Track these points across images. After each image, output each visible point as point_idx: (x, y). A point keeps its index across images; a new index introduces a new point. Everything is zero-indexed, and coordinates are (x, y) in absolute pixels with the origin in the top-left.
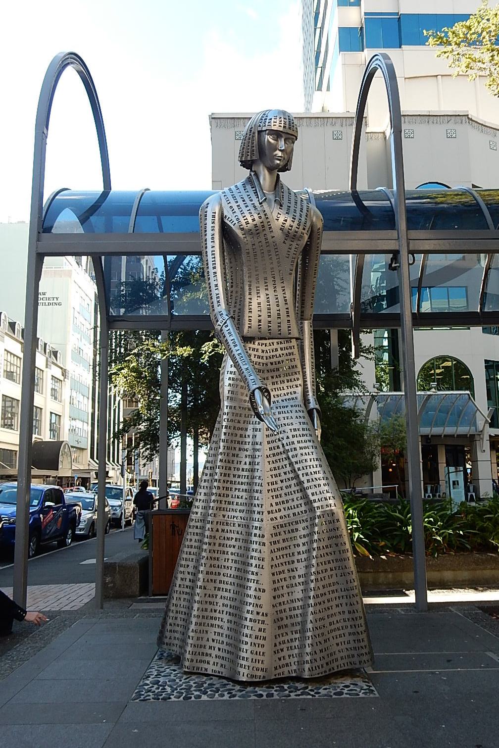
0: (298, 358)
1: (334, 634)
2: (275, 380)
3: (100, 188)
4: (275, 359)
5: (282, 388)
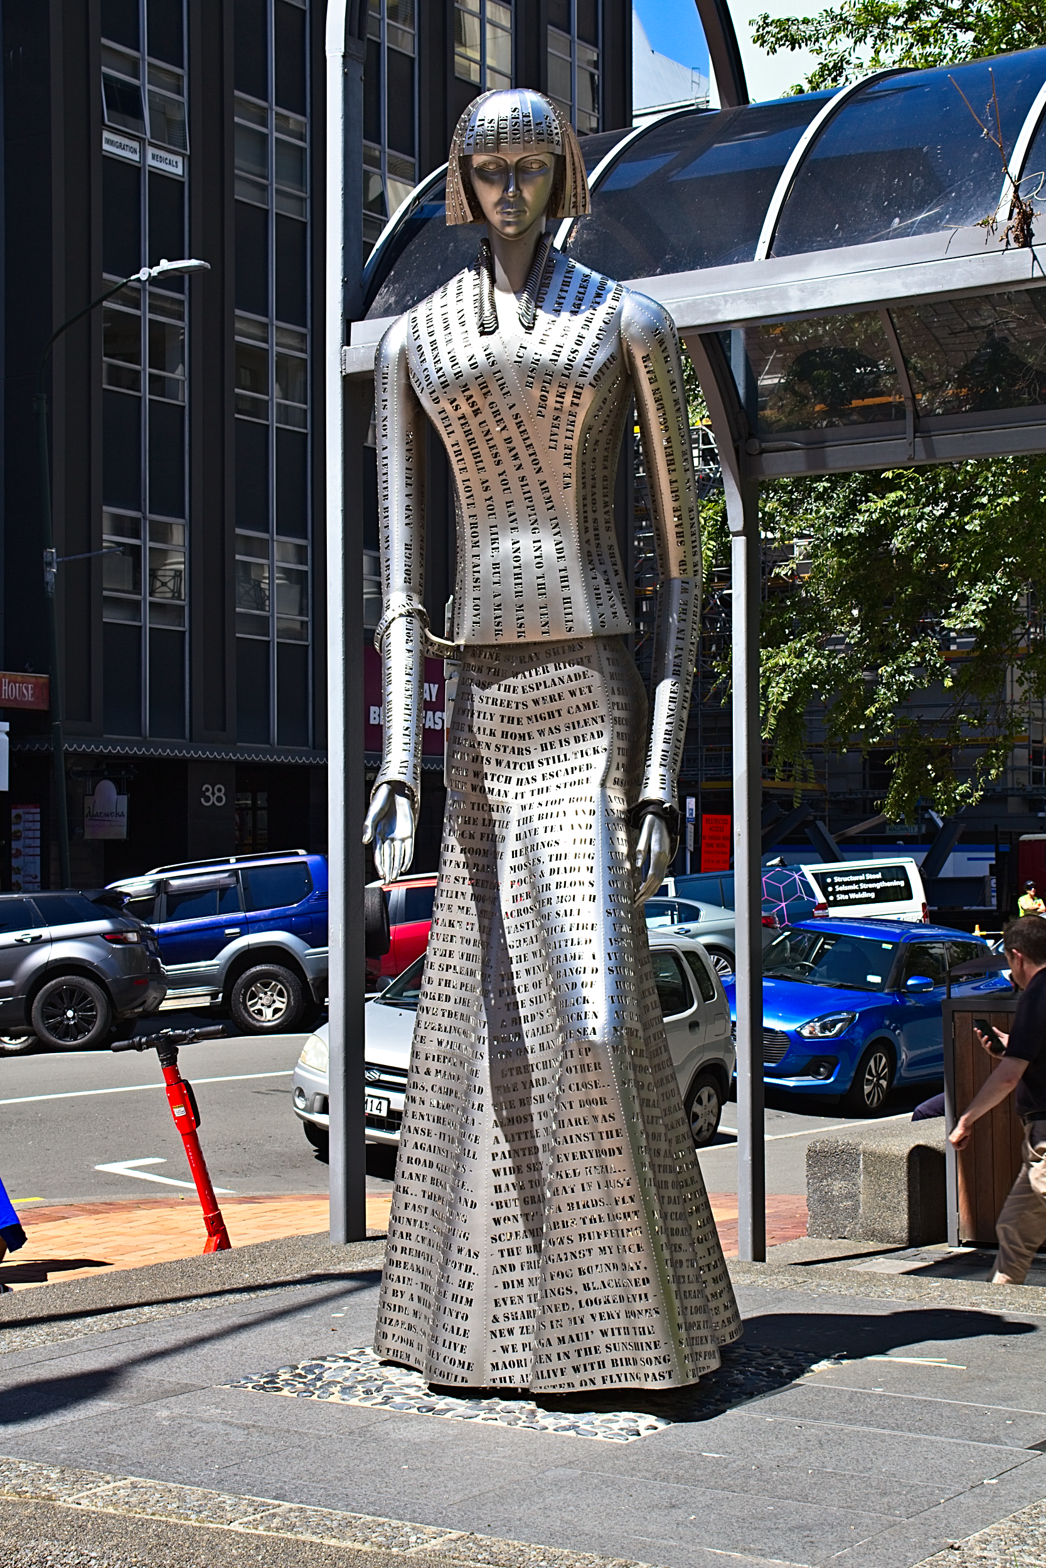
0: (601, 963)
1: (595, 1309)
2: (547, 739)
3: (354, 326)
4: (543, 692)
5: (562, 758)
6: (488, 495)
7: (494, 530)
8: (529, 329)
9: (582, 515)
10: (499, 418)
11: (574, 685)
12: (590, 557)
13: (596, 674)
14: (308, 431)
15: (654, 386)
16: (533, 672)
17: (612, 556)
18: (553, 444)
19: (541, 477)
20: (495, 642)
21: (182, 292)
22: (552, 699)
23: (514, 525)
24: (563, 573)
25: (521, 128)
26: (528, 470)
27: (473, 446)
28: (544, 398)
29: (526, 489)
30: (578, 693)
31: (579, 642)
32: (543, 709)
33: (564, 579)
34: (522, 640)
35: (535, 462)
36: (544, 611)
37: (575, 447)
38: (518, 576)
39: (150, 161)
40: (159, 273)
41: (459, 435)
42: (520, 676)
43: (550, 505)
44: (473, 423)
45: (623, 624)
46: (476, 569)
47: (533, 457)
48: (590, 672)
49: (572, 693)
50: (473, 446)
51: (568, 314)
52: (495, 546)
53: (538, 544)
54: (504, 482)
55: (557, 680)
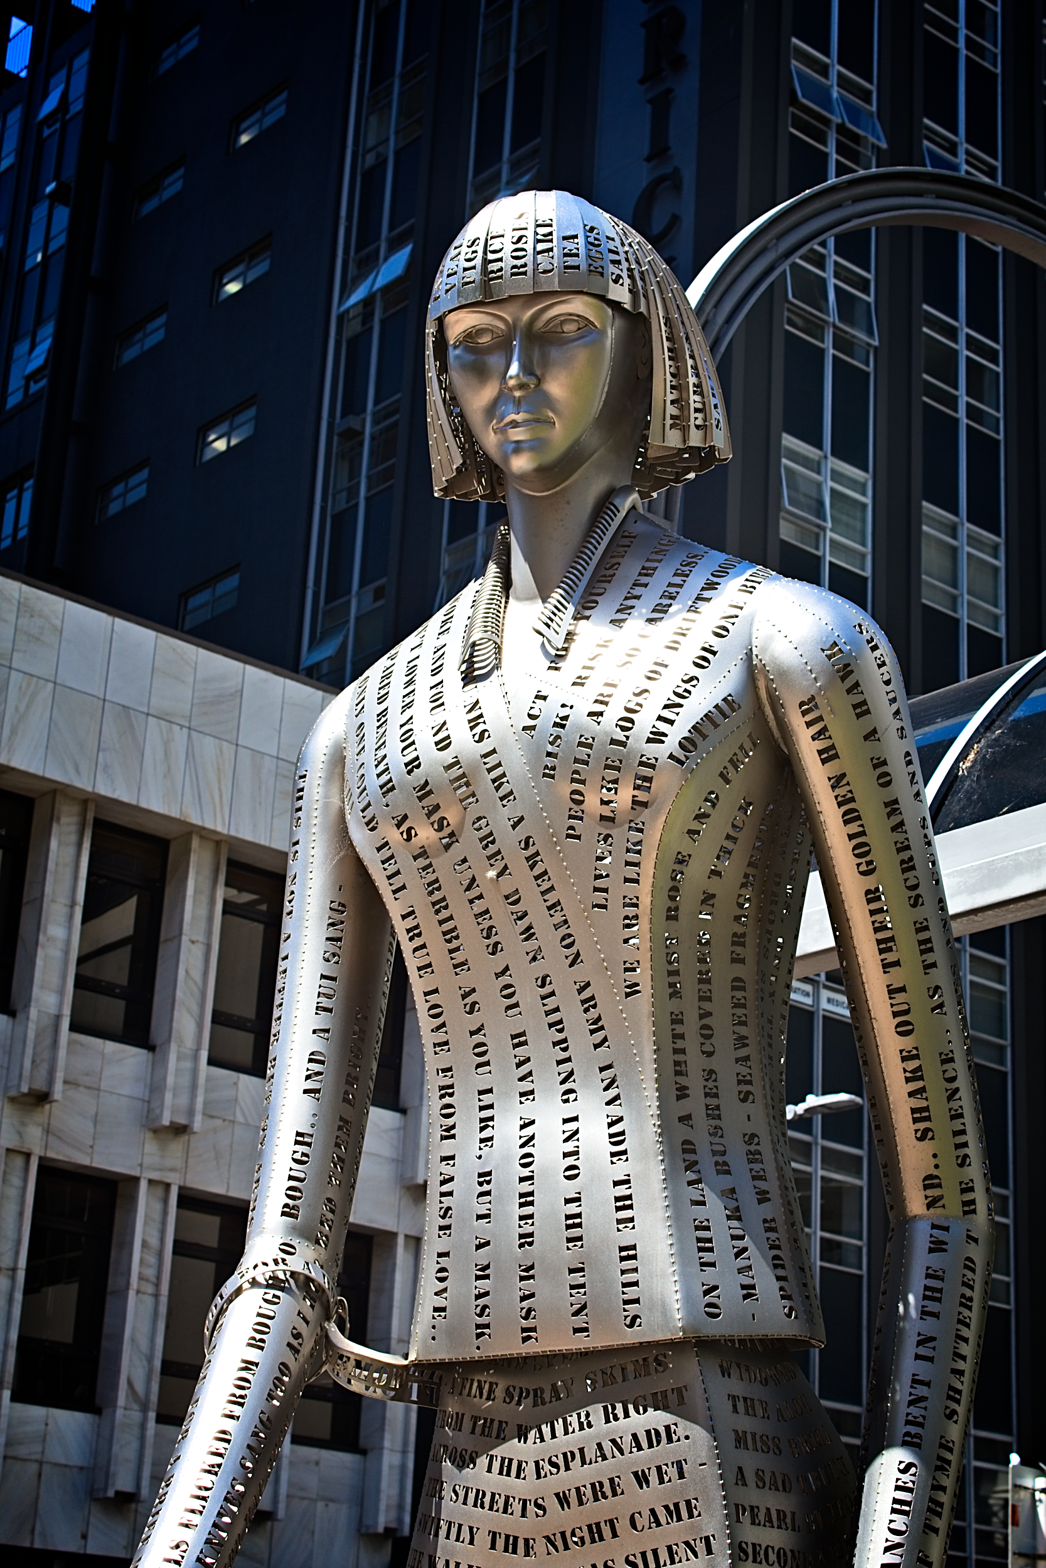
4: (581, 1475)
6: (474, 1021)
7: (487, 1099)
8: (556, 659)
9: (671, 1058)
10: (492, 849)
11: (645, 1458)
12: (684, 1156)
13: (699, 1433)
14: (1012, 1307)
15: (833, 768)
16: (559, 1427)
17: (754, 1157)
18: (599, 897)
19: (581, 973)
20: (477, 1355)
21: (860, 1147)
22: (598, 1492)
23: (526, 1086)
24: (622, 1190)
25: (529, 246)
26: (554, 961)
27: (444, 914)
28: (577, 798)
29: (551, 1003)
30: (653, 1478)
31: (653, 1356)
32: (576, 1517)
33: (624, 1203)
34: (531, 1348)
35: (568, 941)
36: (577, 1278)
37: (646, 901)
38: (526, 1198)
39: (824, 1005)
40: (806, 1111)
41: (416, 896)
42: (532, 1434)
43: (599, 1036)
44: (443, 864)
45: (771, 1313)
46: (446, 1188)
47: (563, 931)
48: (683, 1427)
49: (641, 1479)
50: (444, 914)
51: (641, 623)
52: (486, 1134)
53: (572, 1126)
54: (508, 991)
55: (607, 1446)
